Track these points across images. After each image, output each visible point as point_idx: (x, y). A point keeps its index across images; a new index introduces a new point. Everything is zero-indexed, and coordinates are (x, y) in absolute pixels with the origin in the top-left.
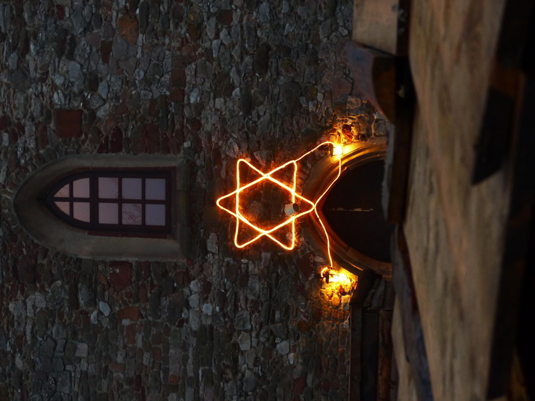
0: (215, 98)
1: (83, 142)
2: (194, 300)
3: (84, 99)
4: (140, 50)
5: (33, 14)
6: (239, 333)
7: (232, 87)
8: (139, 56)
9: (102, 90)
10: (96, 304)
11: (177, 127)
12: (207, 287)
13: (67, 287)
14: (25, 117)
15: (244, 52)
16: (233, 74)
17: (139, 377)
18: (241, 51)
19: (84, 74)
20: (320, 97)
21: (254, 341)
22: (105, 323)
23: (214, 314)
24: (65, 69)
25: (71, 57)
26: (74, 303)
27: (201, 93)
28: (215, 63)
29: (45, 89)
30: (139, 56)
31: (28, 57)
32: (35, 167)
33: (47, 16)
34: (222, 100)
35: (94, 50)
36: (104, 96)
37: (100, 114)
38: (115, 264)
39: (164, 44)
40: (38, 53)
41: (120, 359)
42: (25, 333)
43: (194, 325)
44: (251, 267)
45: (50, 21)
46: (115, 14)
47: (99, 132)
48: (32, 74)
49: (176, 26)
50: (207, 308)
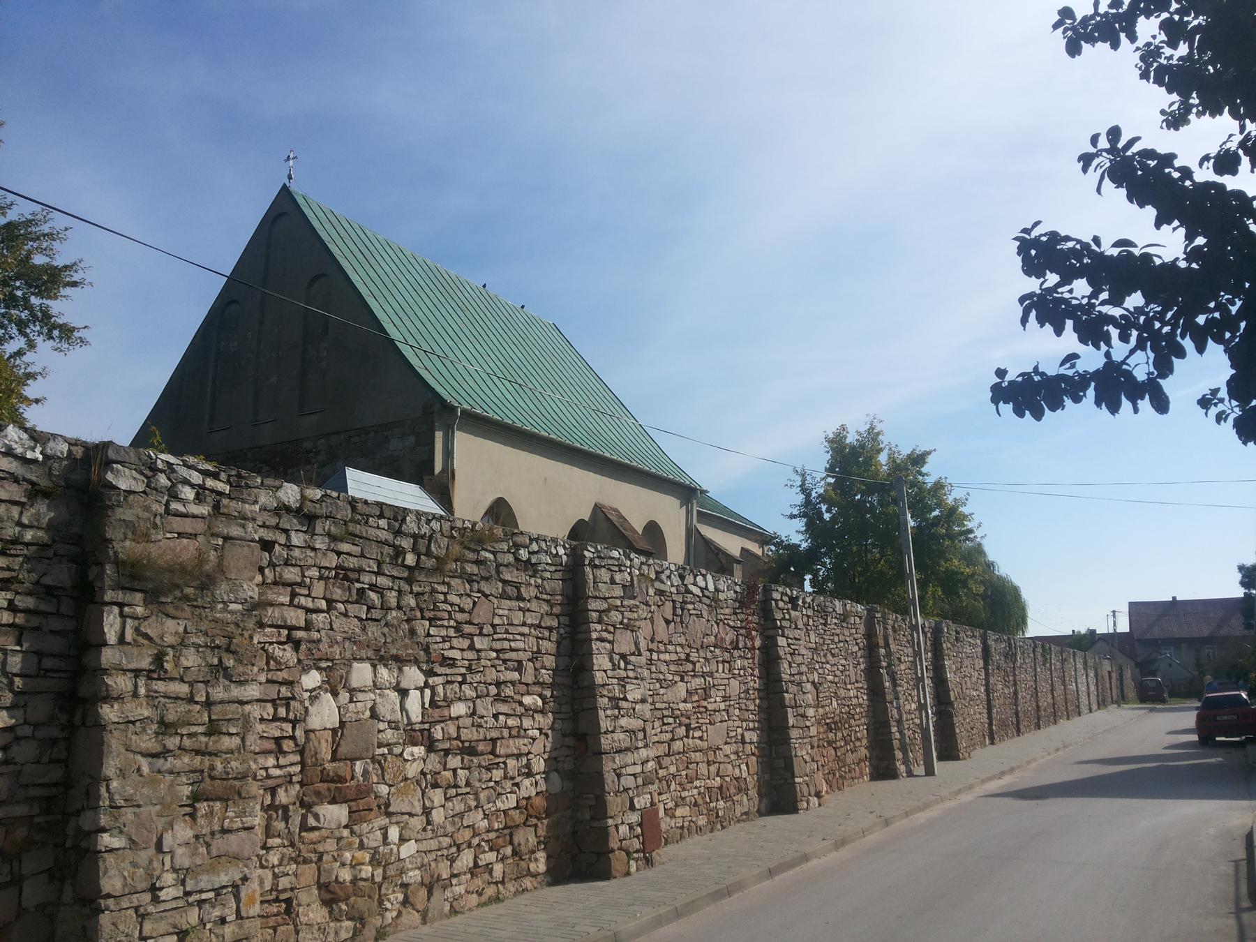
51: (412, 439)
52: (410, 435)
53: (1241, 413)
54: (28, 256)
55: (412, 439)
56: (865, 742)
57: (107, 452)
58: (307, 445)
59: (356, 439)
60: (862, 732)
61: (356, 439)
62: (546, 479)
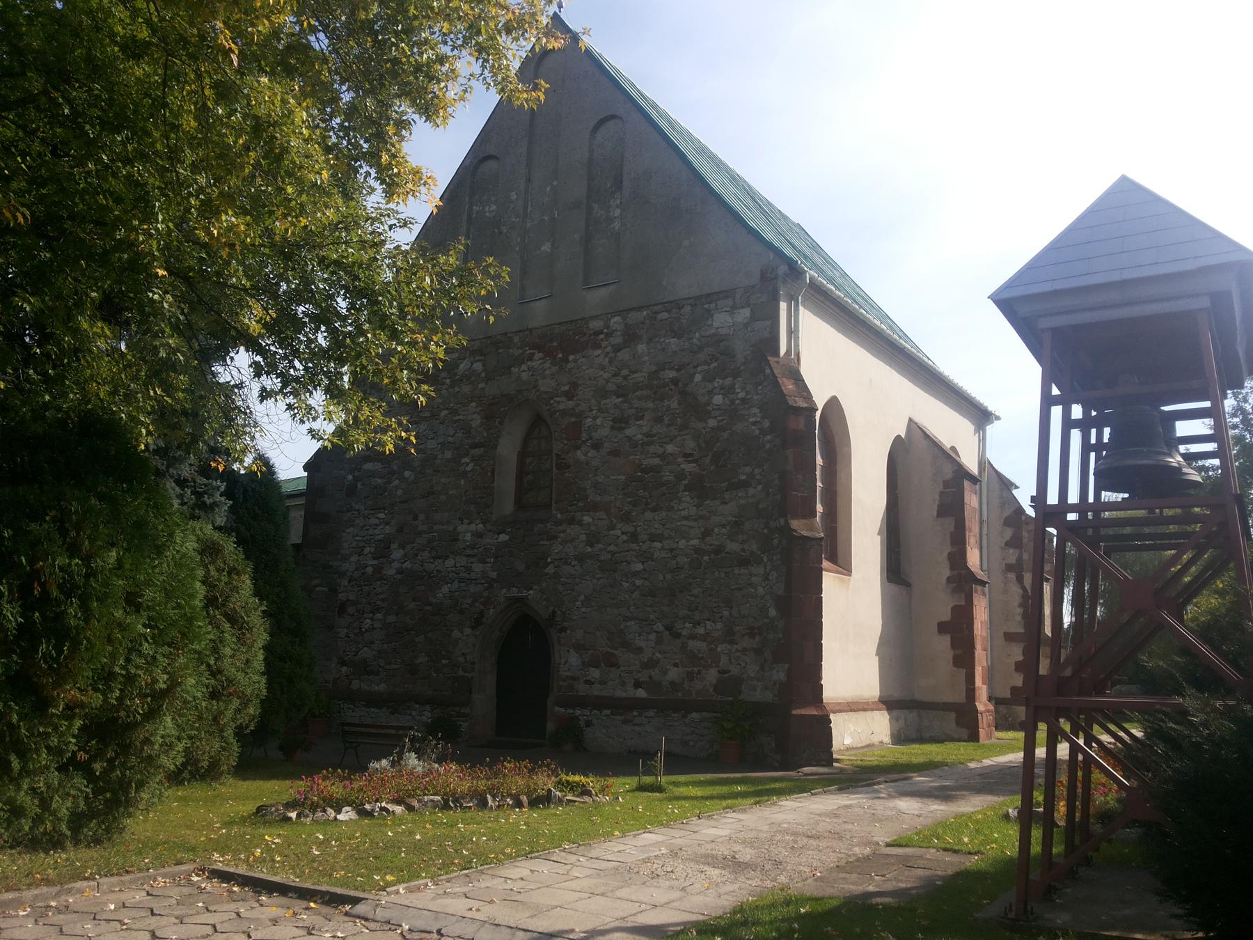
0: (586, 534)
1: (562, 442)
2: (473, 527)
3: (587, 440)
4: (615, 477)
5: (639, 399)
6: (454, 559)
7: (592, 546)
8: (612, 477)
9: (592, 453)
10: (472, 461)
11: (569, 508)
12: (479, 535)
13: (482, 440)
14: (578, 400)
15: (613, 553)
16: (600, 546)
17: (434, 493)
18: (176, 778)
19: (602, 439)
20: (583, 610)
21: (449, 570)
22: (462, 468)
23: (465, 541)
24: (605, 425)
25: (612, 428)
26: (474, 446)
27: (589, 524)
28: (606, 532)
29: (594, 412)
30: (612, 477)
31: (614, 397)
32: (549, 410)
33: (637, 408)
34: (584, 539)
35: (616, 445)
36: (589, 455)
37: (579, 452)
38: (493, 470)
39: (619, 495)
40: (615, 404)
41: (443, 480)
42: (459, 415)
43: (460, 528)
44: (489, 565)
45: (633, 411)
46: (638, 457)
47: (567, 453)
48: (603, 402)
49: (629, 503)
50: (468, 537)
51: (746, 312)
52: (743, 307)
53: (220, 6)
54: (14, 180)
55: (746, 312)
56: (769, 884)
57: (615, 316)
58: (596, 325)
59: (665, 315)
60: (232, 870)
61: (665, 315)
62: (871, 381)
